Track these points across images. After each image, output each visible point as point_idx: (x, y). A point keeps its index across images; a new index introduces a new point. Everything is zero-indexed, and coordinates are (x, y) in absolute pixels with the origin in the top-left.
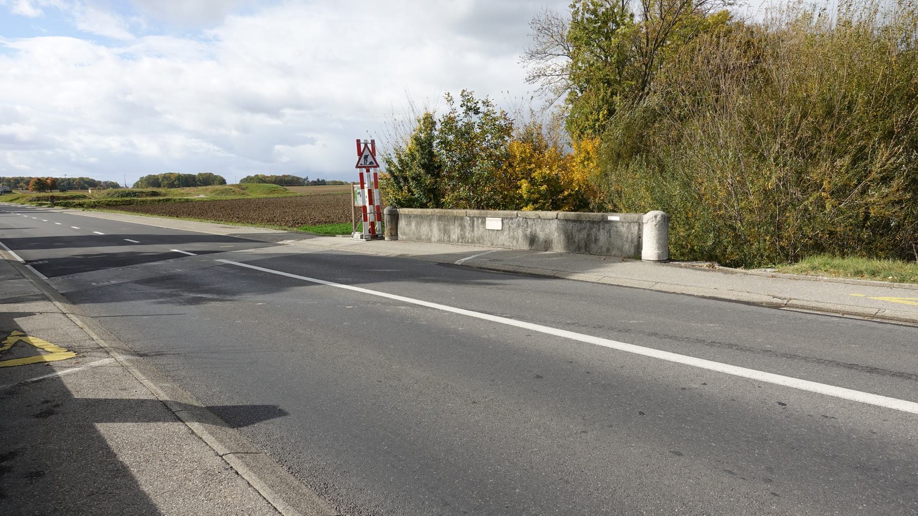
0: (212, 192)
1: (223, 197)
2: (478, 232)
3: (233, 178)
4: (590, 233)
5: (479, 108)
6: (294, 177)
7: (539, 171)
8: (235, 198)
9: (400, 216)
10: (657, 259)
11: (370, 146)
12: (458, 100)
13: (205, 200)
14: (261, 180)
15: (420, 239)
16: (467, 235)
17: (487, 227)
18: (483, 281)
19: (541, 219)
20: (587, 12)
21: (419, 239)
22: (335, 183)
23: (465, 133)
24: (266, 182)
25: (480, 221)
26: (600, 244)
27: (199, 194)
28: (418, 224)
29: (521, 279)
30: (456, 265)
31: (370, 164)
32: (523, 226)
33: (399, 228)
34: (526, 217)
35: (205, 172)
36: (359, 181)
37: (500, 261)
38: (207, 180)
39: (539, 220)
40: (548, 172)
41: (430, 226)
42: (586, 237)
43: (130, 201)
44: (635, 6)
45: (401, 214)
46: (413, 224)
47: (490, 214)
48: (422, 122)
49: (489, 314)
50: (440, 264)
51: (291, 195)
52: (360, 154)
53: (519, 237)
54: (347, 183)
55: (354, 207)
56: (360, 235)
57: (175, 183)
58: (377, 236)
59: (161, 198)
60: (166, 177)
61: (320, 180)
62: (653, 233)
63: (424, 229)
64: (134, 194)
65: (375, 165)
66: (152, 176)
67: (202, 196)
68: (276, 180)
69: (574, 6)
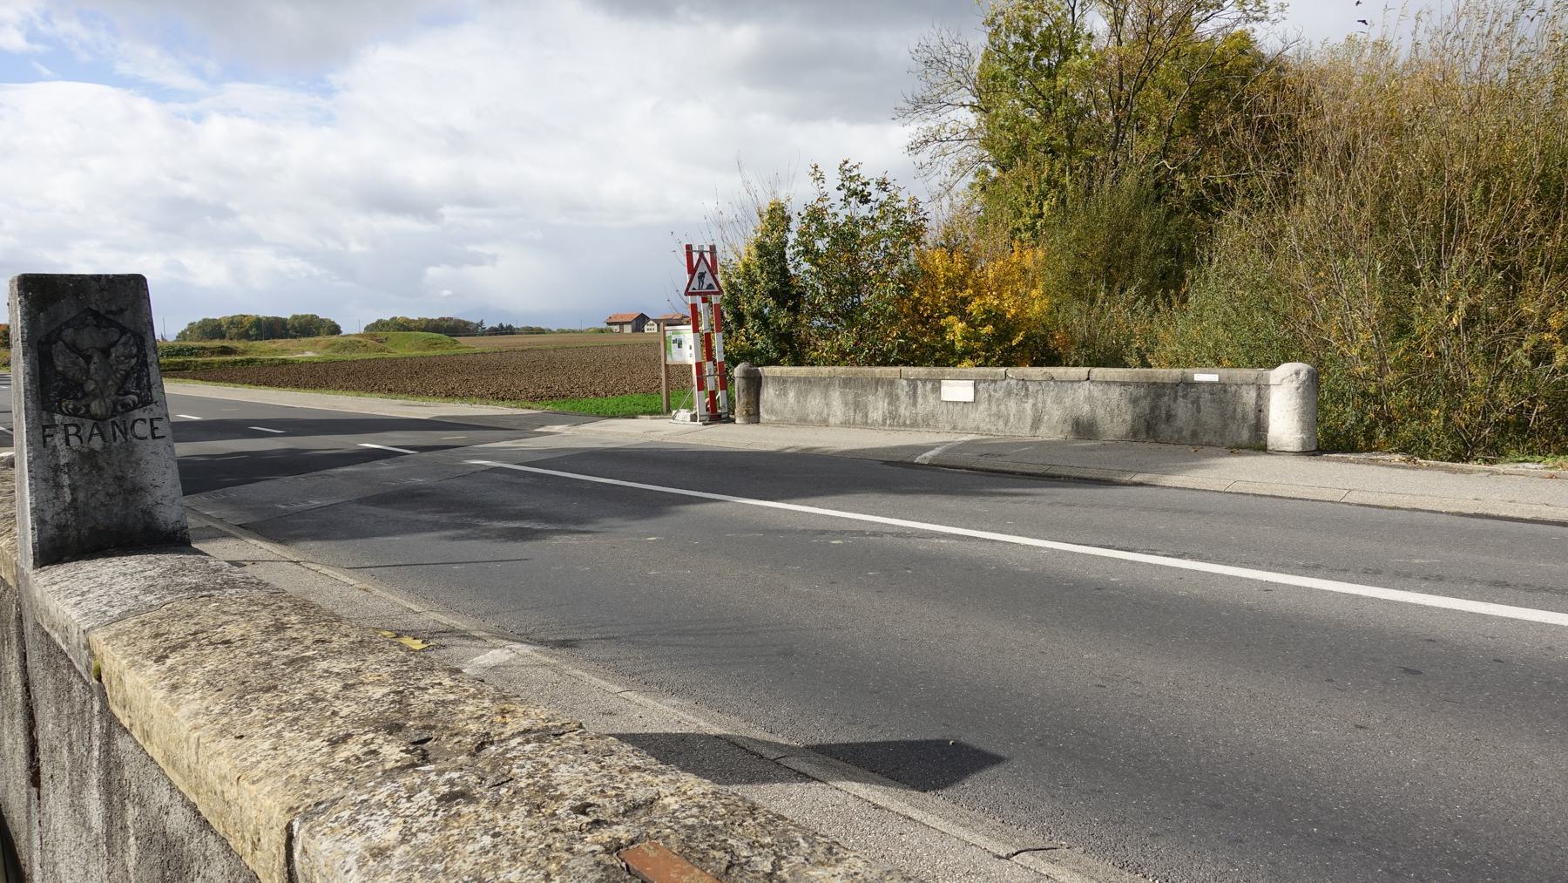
0: (326, 348)
1: (348, 356)
2: (923, 408)
3: (353, 324)
4: (1155, 406)
5: (870, 194)
6: (460, 321)
7: (978, 301)
8: (367, 358)
9: (763, 380)
10: (1300, 449)
11: (708, 256)
12: (833, 179)
13: (315, 360)
14: (403, 326)
15: (805, 421)
16: (902, 411)
17: (944, 398)
18: (1005, 490)
19: (1055, 382)
20: (1015, 33)
21: (803, 421)
22: (530, 331)
23: (846, 238)
24: (410, 330)
25: (929, 386)
26: (1179, 423)
27: (306, 351)
28: (801, 395)
29: (1073, 487)
30: (918, 464)
31: (707, 288)
32: (1017, 394)
33: (761, 401)
34: (1026, 378)
35: (304, 314)
36: (690, 315)
37: (1000, 455)
38: (308, 327)
39: (1052, 383)
40: (996, 302)
41: (826, 396)
42: (1147, 412)
43: (183, 363)
44: (1097, 22)
45: (766, 377)
46: (791, 394)
47: (949, 375)
48: (766, 217)
49: (1125, 550)
50: (886, 463)
51: (465, 351)
52: (692, 270)
53: (1009, 415)
54: (550, 330)
55: (666, 366)
56: (689, 414)
57: (251, 333)
58: (720, 416)
59: (238, 358)
60: (235, 322)
61: (505, 326)
62: (1293, 402)
63: (814, 403)
64: (179, 352)
65: (717, 290)
66: (209, 320)
67: (309, 354)
68: (427, 326)
69: (993, 22)
